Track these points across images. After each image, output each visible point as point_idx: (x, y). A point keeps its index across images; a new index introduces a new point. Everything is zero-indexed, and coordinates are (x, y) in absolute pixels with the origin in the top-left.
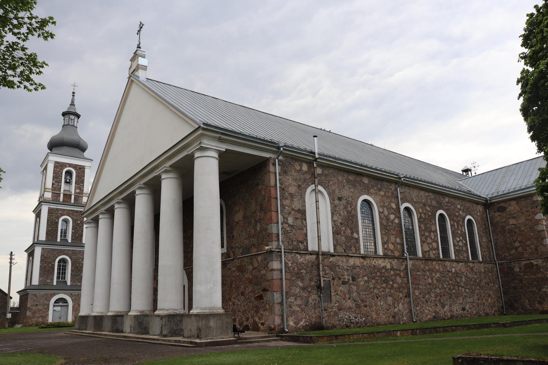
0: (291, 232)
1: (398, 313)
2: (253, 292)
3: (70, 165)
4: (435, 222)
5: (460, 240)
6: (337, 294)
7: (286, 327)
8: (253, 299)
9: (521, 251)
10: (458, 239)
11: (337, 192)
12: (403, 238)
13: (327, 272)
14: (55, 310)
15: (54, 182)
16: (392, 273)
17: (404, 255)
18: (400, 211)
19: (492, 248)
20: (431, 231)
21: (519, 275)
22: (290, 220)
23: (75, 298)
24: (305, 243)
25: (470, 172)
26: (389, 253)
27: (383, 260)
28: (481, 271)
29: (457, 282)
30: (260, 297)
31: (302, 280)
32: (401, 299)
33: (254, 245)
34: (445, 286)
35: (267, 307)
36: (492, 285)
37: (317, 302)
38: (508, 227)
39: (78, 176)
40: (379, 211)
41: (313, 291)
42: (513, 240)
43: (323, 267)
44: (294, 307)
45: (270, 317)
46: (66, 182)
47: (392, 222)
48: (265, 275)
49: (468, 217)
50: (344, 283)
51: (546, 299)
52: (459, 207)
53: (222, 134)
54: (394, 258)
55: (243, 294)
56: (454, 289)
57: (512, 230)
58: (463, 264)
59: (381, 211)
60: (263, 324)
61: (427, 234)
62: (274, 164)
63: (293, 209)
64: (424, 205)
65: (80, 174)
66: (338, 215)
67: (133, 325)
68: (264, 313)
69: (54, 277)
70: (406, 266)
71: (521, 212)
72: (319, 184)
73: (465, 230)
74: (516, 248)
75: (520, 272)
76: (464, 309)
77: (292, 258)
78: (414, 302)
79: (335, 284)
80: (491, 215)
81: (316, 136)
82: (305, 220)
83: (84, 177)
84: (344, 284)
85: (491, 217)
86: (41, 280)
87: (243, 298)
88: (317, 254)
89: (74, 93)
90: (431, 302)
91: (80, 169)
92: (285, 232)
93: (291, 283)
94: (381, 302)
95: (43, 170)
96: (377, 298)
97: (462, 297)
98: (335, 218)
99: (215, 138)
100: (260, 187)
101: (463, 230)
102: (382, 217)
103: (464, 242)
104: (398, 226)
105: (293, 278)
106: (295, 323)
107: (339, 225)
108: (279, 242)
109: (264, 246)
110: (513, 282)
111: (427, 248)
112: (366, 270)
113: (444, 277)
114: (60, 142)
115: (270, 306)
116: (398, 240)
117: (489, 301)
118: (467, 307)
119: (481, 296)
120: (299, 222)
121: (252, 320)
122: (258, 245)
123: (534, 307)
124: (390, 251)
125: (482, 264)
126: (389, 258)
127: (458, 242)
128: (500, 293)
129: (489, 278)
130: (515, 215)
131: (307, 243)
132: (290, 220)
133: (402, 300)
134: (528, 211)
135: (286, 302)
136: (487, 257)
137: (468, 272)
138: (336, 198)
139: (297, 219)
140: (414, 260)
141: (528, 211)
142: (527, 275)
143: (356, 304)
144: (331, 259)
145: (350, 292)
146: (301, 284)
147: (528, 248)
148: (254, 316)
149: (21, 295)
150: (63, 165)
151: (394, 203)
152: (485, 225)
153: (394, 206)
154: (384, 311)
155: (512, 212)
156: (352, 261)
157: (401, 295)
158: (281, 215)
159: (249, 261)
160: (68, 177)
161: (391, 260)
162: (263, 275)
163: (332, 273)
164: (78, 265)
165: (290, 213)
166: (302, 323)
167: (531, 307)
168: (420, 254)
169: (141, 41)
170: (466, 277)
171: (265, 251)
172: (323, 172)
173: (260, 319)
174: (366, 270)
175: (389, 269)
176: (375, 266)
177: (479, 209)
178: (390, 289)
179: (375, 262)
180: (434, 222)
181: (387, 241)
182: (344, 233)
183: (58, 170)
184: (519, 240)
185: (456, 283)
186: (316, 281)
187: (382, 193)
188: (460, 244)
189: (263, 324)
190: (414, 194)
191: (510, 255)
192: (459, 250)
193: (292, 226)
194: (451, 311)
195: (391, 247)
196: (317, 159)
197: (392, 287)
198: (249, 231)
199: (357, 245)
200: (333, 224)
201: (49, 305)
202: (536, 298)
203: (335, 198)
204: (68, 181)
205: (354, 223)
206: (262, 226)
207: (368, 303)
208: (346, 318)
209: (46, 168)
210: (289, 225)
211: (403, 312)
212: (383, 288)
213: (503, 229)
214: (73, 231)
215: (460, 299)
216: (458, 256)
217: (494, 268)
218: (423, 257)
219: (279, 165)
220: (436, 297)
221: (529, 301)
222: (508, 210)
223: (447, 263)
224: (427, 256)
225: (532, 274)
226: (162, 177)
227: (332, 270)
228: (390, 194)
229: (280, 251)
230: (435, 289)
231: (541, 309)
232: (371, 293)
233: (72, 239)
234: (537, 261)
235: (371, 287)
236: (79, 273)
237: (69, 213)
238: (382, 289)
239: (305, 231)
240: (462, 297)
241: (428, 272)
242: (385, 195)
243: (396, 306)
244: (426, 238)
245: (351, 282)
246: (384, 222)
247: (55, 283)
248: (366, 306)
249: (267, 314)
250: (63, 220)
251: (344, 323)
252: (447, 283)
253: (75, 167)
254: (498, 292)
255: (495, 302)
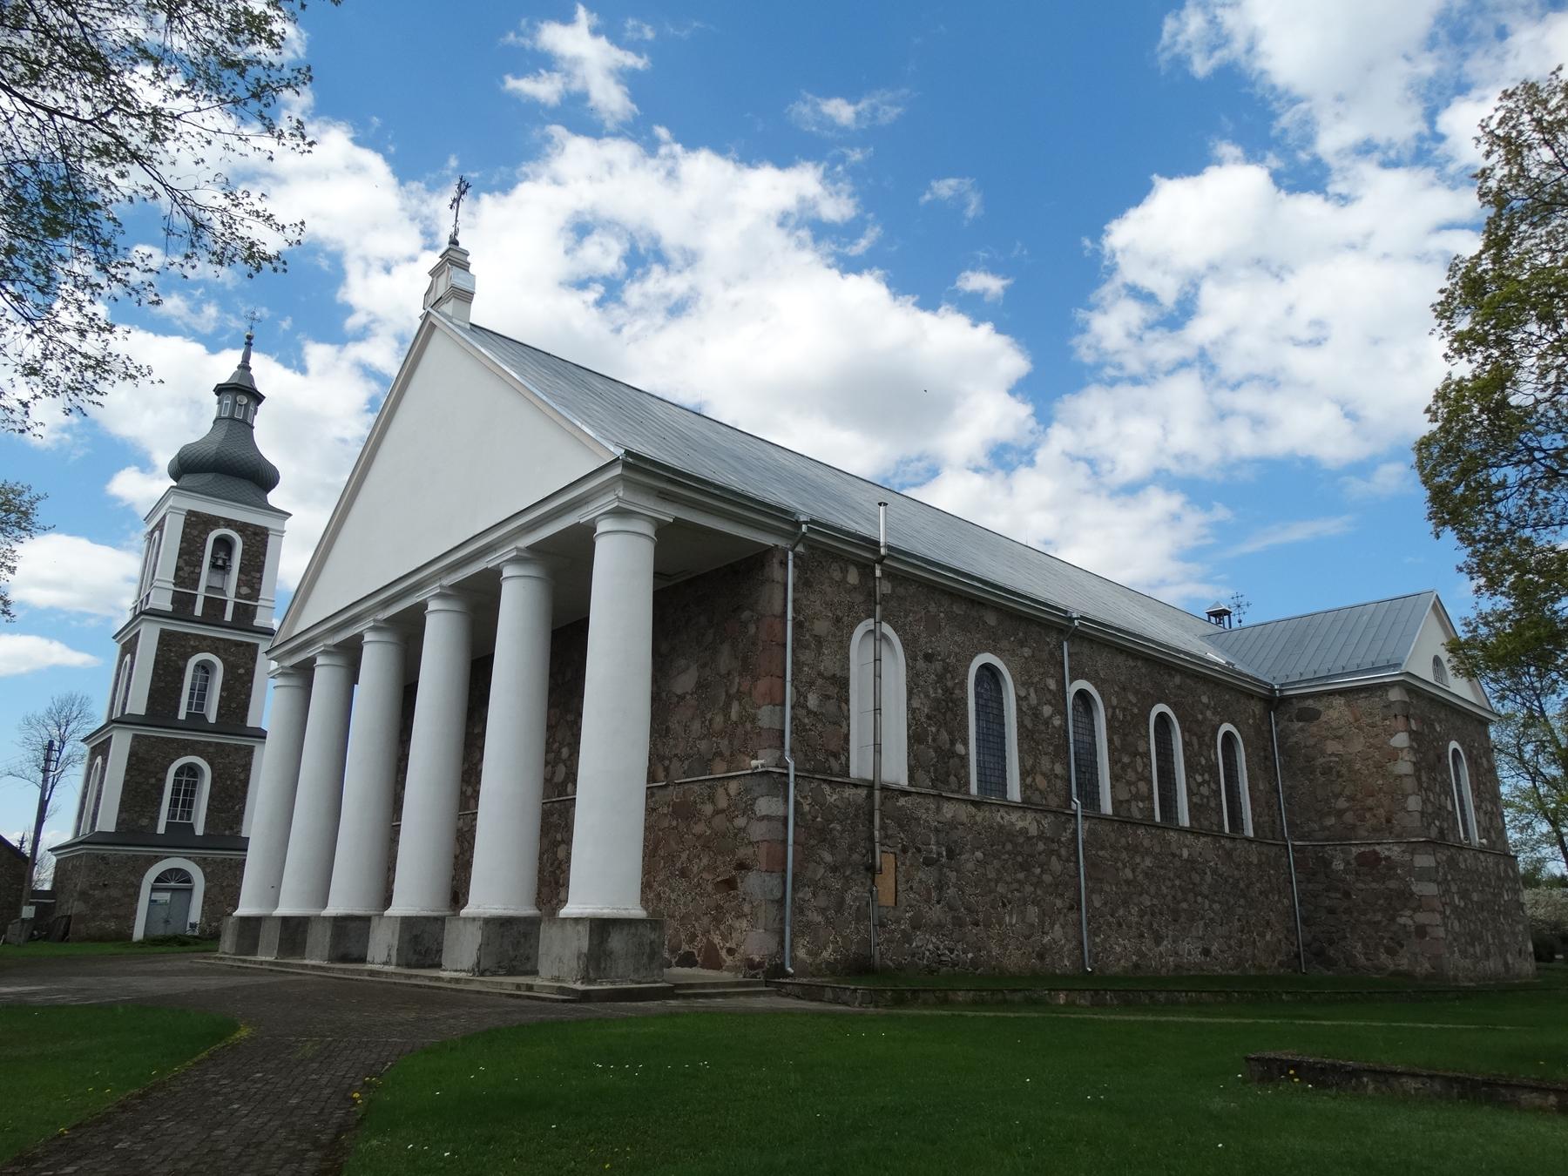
0: (813, 728)
1: (1051, 949)
2: (711, 868)
3: (229, 523)
4: (1148, 732)
5: (1204, 782)
6: (911, 887)
7: (787, 963)
8: (710, 888)
9: (1351, 822)
10: (1199, 779)
11: (923, 641)
12: (1069, 767)
13: (890, 832)
14: (155, 901)
15: (182, 564)
16: (1041, 846)
17: (1070, 805)
18: (1065, 698)
19: (1280, 809)
20: (1135, 754)
21: (1343, 880)
22: (813, 701)
23: (213, 871)
24: (843, 758)
25: (1226, 617)
26: (1036, 798)
27: (1020, 813)
28: (1251, 863)
29: (1194, 884)
30: (730, 884)
31: (833, 847)
32: (1060, 913)
33: (719, 754)
34: (1165, 891)
35: (746, 908)
36: (1276, 898)
37: (864, 903)
38: (1321, 760)
39: (247, 553)
40: (1016, 694)
41: (855, 876)
42: (1332, 792)
43: (882, 819)
44: (810, 913)
45: (751, 934)
46: (214, 566)
47: (1047, 722)
48: (744, 829)
49: (1226, 727)
50: (928, 862)
51: (1405, 943)
52: (1205, 699)
53: (670, 481)
54: (1045, 811)
55: (684, 873)
56: (1185, 900)
57: (1331, 768)
58: (1208, 839)
59: (1023, 694)
60: (730, 951)
61: (1126, 760)
62: (784, 564)
63: (820, 674)
64: (1124, 689)
65: (255, 549)
66: (922, 696)
67: (396, 943)
68: (737, 924)
69: (159, 813)
70: (1075, 831)
71: (1356, 725)
72: (883, 618)
73: (1217, 758)
74: (1340, 813)
75: (1345, 871)
76: (1206, 952)
77: (811, 791)
78: (1089, 924)
79: (908, 863)
80: (1280, 727)
81: (885, 504)
82: (847, 701)
83: (265, 555)
84: (927, 866)
85: (1282, 731)
86: (124, 820)
87: (684, 884)
88: (870, 786)
89: (249, 338)
90: (1130, 927)
91: (255, 534)
92: (798, 728)
93: (806, 855)
94: (1011, 916)
95: (152, 532)
96: (1004, 905)
97: (1202, 922)
98: (915, 704)
99: (652, 488)
100: (746, 615)
101: (1213, 757)
102: (1024, 709)
103: (1213, 786)
104: (1060, 735)
105: (812, 842)
106: (809, 953)
107: (923, 719)
108: (783, 752)
109: (747, 759)
110: (1327, 896)
111: (1124, 796)
112: (979, 834)
113: (1162, 868)
114: (204, 460)
115: (753, 907)
116: (1058, 769)
117: (1268, 937)
118: (1214, 948)
119: (1247, 922)
120: (831, 706)
121: (705, 940)
122: (732, 755)
123: (1376, 962)
124: (1037, 792)
125: (1254, 846)
126: (1036, 811)
127: (1199, 785)
128: (1293, 918)
129: (1269, 881)
130: (1341, 732)
131: (848, 759)
132: (813, 701)
133: (1062, 916)
134: (1373, 726)
135: (793, 899)
136: (1267, 829)
137: (1219, 863)
138: (920, 655)
139: (828, 697)
140: (1094, 821)
141: (1373, 726)
142: (1364, 882)
143: (953, 917)
144: (902, 801)
145: (940, 887)
146: (828, 858)
147: (1368, 815)
148: (709, 932)
149: (60, 857)
150: (212, 522)
151: (1052, 676)
152: (1265, 750)
153: (1052, 685)
154: (1018, 939)
155: (1334, 725)
156: (949, 810)
157: (1059, 903)
158: (792, 685)
159: (706, 793)
160: (222, 555)
161: (1038, 816)
162: (740, 829)
163: (902, 835)
164: (229, 782)
165: (811, 684)
166: (825, 954)
167: (1368, 959)
168: (1107, 807)
169: (460, 226)
170: (1214, 871)
171: (749, 772)
172: (893, 590)
173: (724, 938)
174: (979, 834)
175: (1034, 837)
176: (1001, 827)
177: (1253, 710)
178: (1036, 885)
179: (1002, 818)
180: (1143, 732)
181: (1033, 767)
182: (934, 740)
183: (195, 533)
184: (1347, 792)
185: (1191, 886)
186: (864, 851)
187: (1027, 652)
188: (1204, 790)
189: (730, 951)
190: (1102, 660)
191: (1323, 828)
192: (1201, 806)
193: (815, 714)
194: (1176, 953)
195: (1041, 782)
196: (884, 557)
197: (1038, 883)
198: (711, 720)
199: (963, 773)
200: (910, 716)
201: (139, 887)
202: (1382, 938)
203: (916, 656)
204: (220, 562)
205: (959, 718)
206: (744, 708)
207: (981, 916)
208: (929, 950)
209: (160, 526)
210: (809, 712)
211: (1062, 947)
212: (1019, 881)
213: (1310, 762)
214: (224, 694)
215: (1197, 926)
216: (1198, 820)
217: (1281, 857)
218: (1114, 815)
219: (795, 566)
220: (1141, 917)
221: (1365, 945)
222: (1323, 718)
223: (1172, 834)
224: (1123, 813)
225: (1374, 881)
226: (505, 574)
227: (901, 826)
228: (1045, 656)
229: (785, 772)
230: (1141, 895)
231: (1392, 967)
232: (990, 892)
233: (219, 715)
234: (1389, 849)
235: (989, 877)
236: (230, 805)
237: (215, 646)
238: (1015, 886)
239: (844, 730)
240: (1202, 922)
241: (1125, 853)
242: (1033, 656)
243: (1045, 930)
244: (1124, 767)
245: (944, 860)
246: (1028, 723)
247: (161, 829)
248: (977, 924)
249: (744, 924)
250: (197, 665)
251: (925, 962)
252: (1169, 883)
253: (242, 528)
254: (1289, 917)
255: (1280, 941)
